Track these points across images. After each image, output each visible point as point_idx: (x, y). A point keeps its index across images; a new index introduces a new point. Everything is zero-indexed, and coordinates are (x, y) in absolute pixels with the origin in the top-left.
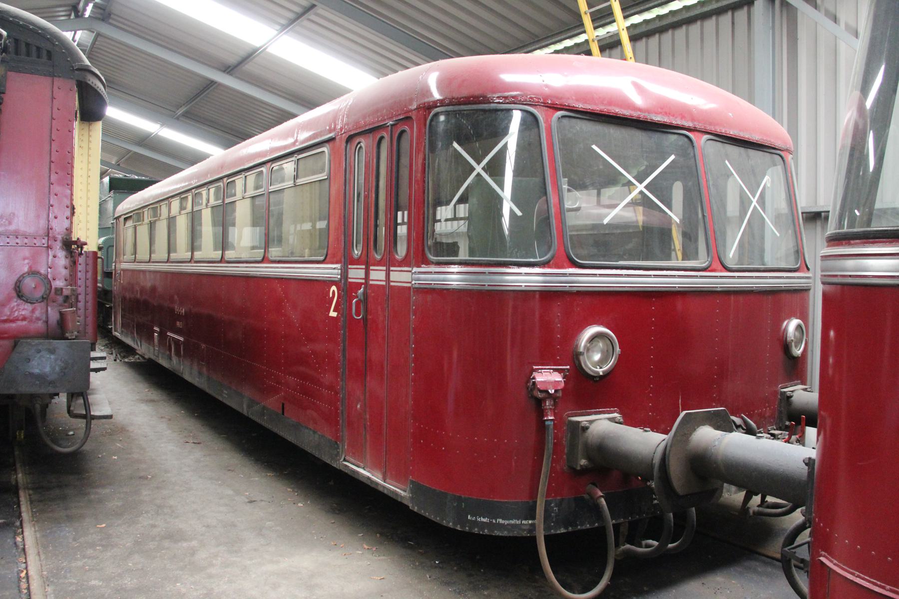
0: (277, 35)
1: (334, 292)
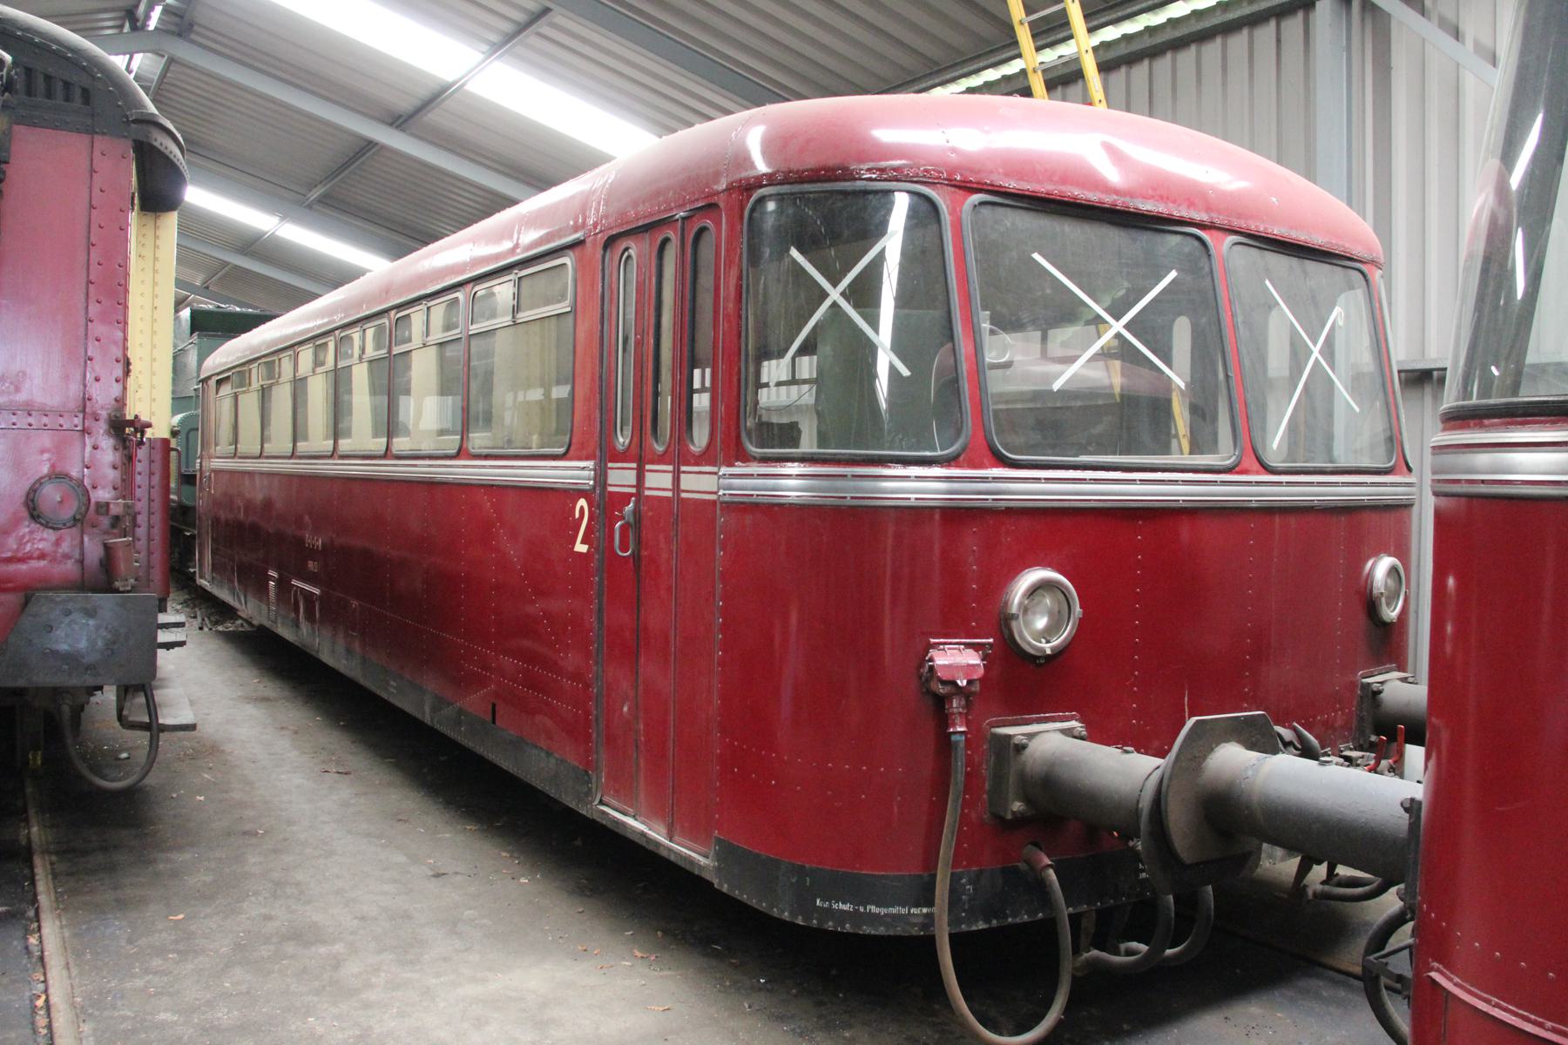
0: (484, 61)
1: (582, 509)
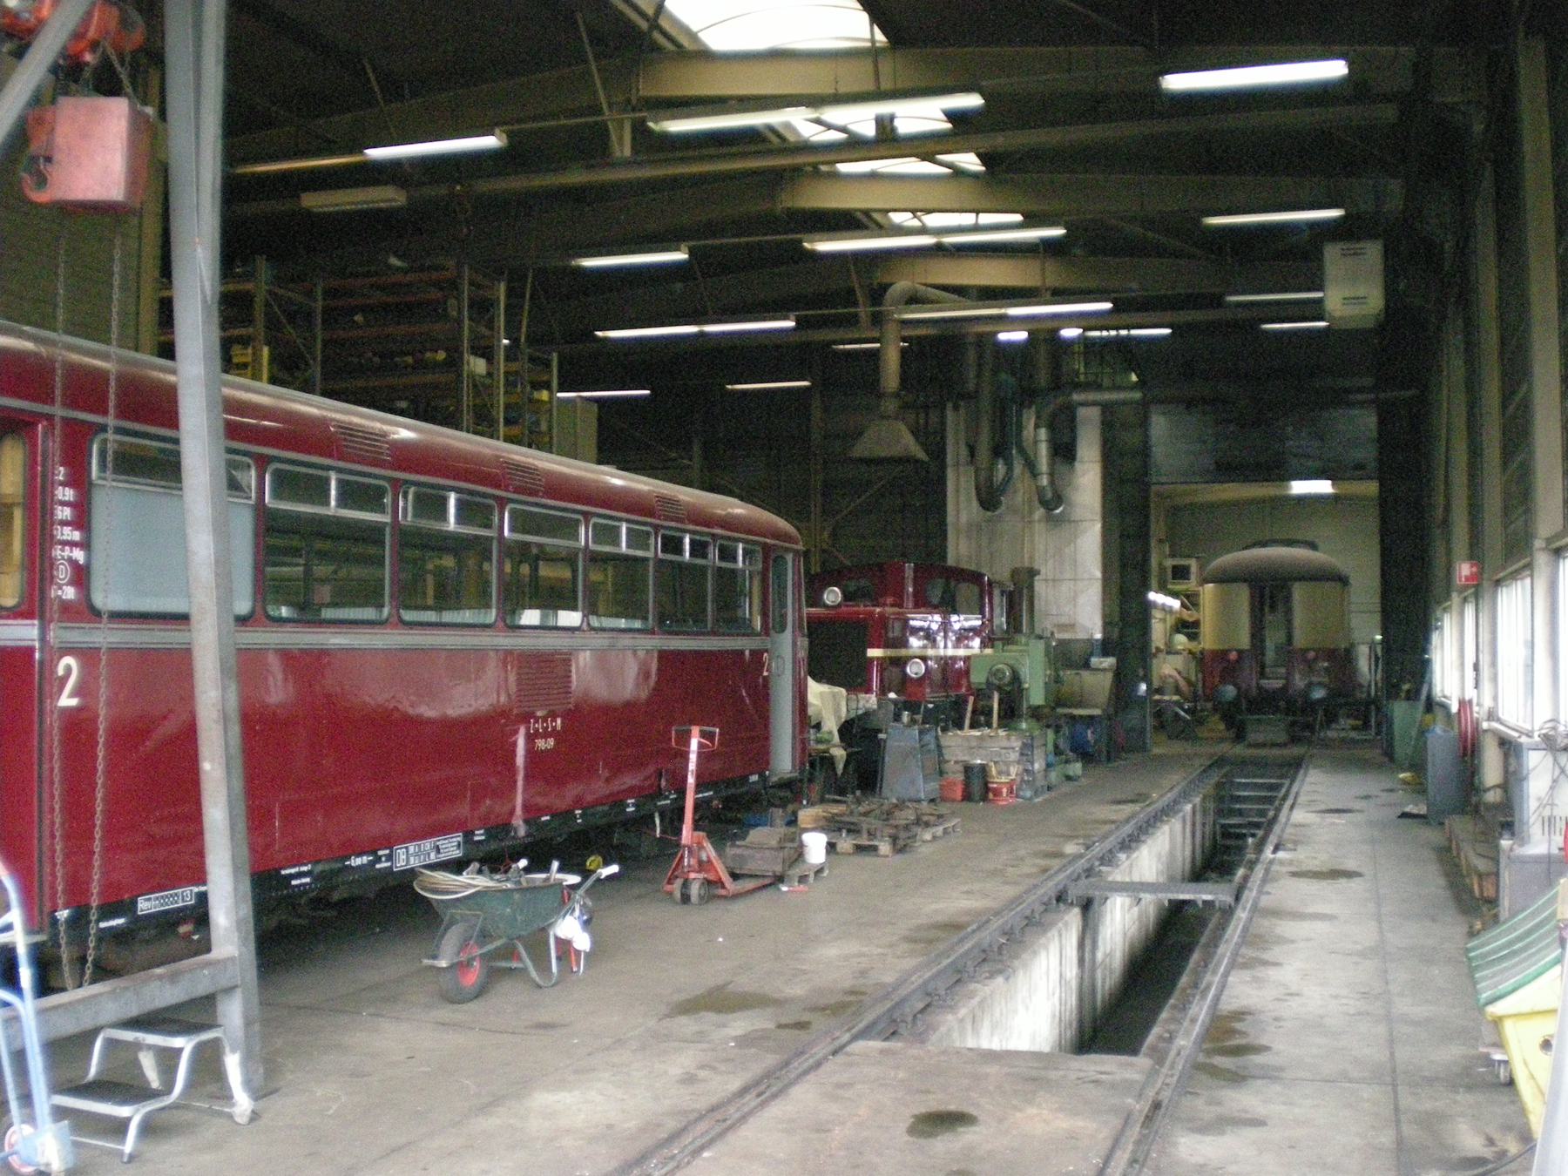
1: (68, 670)
